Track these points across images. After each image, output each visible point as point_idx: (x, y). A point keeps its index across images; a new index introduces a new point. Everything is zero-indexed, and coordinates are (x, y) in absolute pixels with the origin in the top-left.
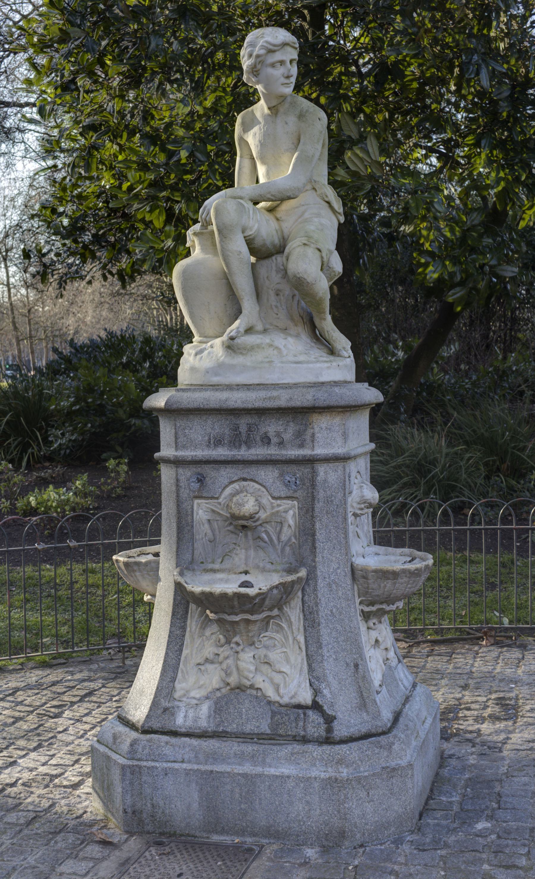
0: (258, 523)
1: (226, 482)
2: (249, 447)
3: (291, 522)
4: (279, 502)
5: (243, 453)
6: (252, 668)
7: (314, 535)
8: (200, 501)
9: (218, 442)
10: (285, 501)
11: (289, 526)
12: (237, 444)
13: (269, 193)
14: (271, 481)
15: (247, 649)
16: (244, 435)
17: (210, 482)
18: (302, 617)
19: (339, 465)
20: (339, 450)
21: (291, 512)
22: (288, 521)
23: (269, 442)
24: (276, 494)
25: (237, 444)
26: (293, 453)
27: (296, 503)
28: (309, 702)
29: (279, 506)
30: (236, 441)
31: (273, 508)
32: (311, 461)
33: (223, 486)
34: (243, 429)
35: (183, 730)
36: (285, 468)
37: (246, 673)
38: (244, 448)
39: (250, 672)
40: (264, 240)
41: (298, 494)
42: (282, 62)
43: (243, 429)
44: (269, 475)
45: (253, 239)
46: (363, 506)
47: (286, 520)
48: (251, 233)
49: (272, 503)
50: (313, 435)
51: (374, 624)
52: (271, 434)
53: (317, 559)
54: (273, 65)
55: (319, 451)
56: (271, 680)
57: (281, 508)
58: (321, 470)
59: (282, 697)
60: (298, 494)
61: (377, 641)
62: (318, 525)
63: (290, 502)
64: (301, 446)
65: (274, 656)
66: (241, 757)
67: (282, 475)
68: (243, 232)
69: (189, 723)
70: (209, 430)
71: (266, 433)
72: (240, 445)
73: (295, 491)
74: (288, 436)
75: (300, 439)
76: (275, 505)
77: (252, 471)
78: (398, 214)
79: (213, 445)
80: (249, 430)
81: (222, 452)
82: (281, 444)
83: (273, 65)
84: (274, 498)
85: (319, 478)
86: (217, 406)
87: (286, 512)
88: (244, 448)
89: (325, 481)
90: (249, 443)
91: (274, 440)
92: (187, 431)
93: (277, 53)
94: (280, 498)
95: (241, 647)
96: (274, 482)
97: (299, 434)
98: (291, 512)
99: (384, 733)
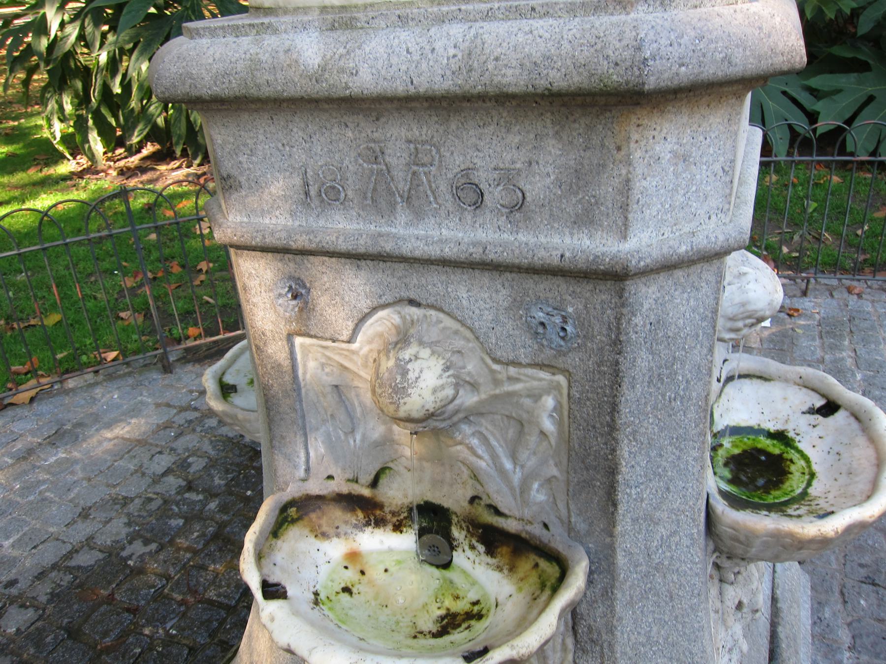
2: (419, 215)
3: (548, 425)
4: (512, 371)
5: (410, 234)
7: (612, 471)
8: (308, 341)
10: (530, 371)
11: (543, 433)
12: (383, 204)
14: (488, 316)
16: (399, 174)
22: (538, 424)
23: (479, 201)
25: (383, 204)
26: (556, 240)
27: (561, 379)
29: (510, 379)
30: (379, 196)
32: (614, 277)
34: (397, 156)
36: (530, 284)
38: (402, 216)
41: (573, 360)
43: (397, 156)
44: (480, 299)
49: (492, 372)
52: (482, 177)
55: (642, 242)
57: (518, 387)
60: (573, 360)
62: (625, 450)
64: (586, 219)
66: (498, 441)
67: (517, 304)
70: (299, 156)
71: (467, 172)
72: (393, 206)
73: (560, 353)
74: (537, 186)
75: (594, 198)
76: (502, 376)
77: (434, 284)
78: (421, 343)
79: (316, 202)
80: (415, 160)
81: (343, 227)
82: (518, 208)
84: (496, 360)
85: (638, 320)
86: (577, 80)
87: (536, 397)
88: (402, 216)
89: (659, 323)
90: (415, 201)
91: (495, 195)
92: (243, 159)
96: (496, 320)
97: (578, 180)
98: (549, 402)
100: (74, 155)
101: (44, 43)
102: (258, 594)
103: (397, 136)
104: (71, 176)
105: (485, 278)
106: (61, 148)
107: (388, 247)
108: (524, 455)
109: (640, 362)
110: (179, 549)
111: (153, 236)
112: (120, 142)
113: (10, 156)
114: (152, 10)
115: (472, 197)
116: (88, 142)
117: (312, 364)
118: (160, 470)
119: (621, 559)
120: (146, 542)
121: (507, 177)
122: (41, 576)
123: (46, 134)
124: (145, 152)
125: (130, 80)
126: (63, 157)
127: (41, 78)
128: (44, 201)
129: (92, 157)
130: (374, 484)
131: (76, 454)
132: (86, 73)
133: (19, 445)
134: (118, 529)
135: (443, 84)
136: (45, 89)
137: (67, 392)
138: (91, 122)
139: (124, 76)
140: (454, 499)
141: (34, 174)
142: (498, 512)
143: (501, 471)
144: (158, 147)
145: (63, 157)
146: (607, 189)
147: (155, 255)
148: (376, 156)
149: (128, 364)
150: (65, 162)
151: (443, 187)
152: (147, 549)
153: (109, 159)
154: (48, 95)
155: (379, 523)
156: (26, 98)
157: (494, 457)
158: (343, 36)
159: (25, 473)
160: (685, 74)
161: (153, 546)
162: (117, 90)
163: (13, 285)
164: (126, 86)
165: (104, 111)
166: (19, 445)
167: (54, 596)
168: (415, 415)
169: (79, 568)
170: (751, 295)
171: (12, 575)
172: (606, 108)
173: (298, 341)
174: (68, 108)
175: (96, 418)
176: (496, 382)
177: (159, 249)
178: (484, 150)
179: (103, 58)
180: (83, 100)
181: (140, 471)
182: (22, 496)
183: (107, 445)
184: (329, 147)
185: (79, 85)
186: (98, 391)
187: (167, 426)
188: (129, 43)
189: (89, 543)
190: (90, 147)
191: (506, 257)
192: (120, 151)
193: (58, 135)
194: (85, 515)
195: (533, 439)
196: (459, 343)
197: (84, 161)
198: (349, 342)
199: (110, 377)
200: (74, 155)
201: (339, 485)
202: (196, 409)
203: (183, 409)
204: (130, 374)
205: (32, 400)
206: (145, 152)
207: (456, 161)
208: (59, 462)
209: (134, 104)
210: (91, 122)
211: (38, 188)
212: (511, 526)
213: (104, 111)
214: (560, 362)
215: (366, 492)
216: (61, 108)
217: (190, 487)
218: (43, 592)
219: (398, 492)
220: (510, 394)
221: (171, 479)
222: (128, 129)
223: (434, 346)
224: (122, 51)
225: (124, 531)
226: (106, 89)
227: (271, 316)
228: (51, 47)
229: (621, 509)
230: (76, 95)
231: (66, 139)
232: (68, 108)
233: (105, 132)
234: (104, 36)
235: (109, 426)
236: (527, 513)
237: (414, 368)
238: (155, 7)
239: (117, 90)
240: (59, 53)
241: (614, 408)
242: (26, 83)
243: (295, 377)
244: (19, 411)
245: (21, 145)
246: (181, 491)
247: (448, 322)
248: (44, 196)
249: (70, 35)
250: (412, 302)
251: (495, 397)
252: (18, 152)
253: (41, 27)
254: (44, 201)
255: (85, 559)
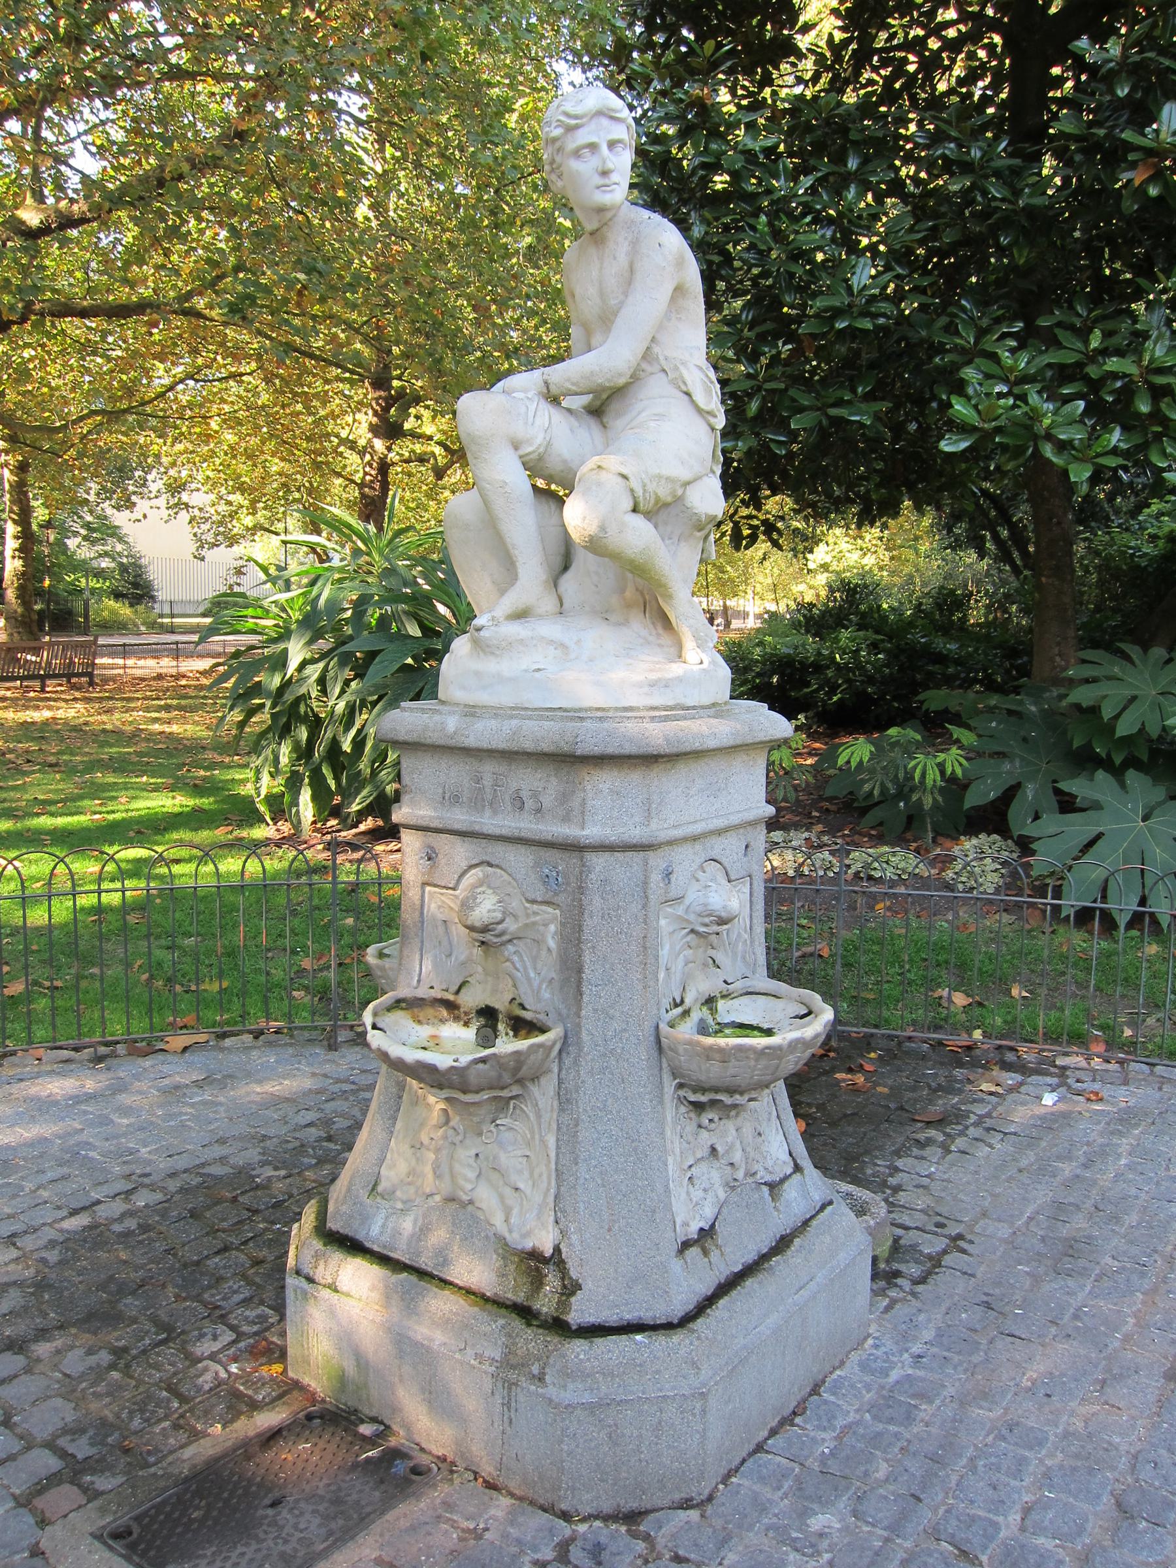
0: (505, 938)
1: (464, 865)
2: (495, 813)
3: (552, 943)
5: (490, 823)
6: (471, 1175)
7: (580, 971)
9: (455, 799)
10: (543, 908)
11: (549, 950)
13: (568, 380)
14: (523, 871)
15: (467, 1141)
16: (488, 790)
17: (443, 862)
18: (556, 1103)
19: (637, 857)
20: (635, 833)
21: (552, 928)
24: (531, 896)
28: (548, 1252)
30: (478, 802)
31: (528, 916)
33: (460, 871)
34: (487, 781)
35: (376, 1248)
37: (462, 1182)
38: (488, 812)
39: (467, 1180)
40: (565, 462)
42: (593, 147)
44: (519, 860)
45: (541, 458)
46: (707, 920)
47: (544, 941)
48: (530, 449)
50: (583, 802)
51: (711, 1121)
52: (525, 794)
53: (583, 1013)
54: (577, 153)
55: (592, 832)
56: (502, 1198)
58: (599, 862)
59: (510, 1231)
60: (561, 899)
61: (713, 1150)
62: (587, 958)
63: (550, 910)
64: (566, 819)
65: (510, 1159)
67: (537, 864)
68: (516, 448)
69: (385, 1238)
73: (556, 894)
74: (547, 800)
77: (499, 852)
78: (489, 887)
81: (460, 818)
83: (577, 153)
84: (528, 901)
88: (488, 812)
90: (494, 805)
91: (529, 804)
93: (581, 131)
94: (533, 902)
95: (460, 1138)
97: (564, 798)
98: (552, 928)
99: (669, 1327)
100: (275, 820)
101: (276, 681)
102: (369, 1028)
103: (489, 769)
104: (267, 842)
105: (522, 849)
106: (262, 808)
107: (477, 828)
108: (539, 965)
109: (595, 902)
110: (305, 1180)
111: (350, 921)
112: (336, 812)
113: (197, 811)
114: (410, 661)
115: (518, 804)
116: (297, 805)
117: (433, 906)
118: (303, 1122)
119: (585, 1036)
120: (276, 1169)
121: (535, 795)
122: (173, 1175)
123: (248, 790)
124: (362, 827)
125: (365, 737)
126: (262, 820)
127: (263, 719)
128: (231, 865)
129: (297, 826)
130: (457, 992)
131: (221, 1099)
132: (316, 724)
133: (166, 1082)
134: (253, 1154)
135: (502, 746)
136: (263, 735)
137: (222, 1049)
138: (307, 780)
139: (359, 731)
140: (500, 1003)
141: (220, 834)
142: (524, 1008)
143: (529, 979)
144: (380, 823)
145: (262, 820)
146: (575, 803)
147: (347, 939)
148: (478, 780)
149: (292, 1036)
150: (263, 826)
151: (507, 798)
152: (277, 1173)
153: (316, 830)
154: (264, 743)
155: (457, 1019)
156: (231, 747)
157: (525, 968)
158: (468, 719)
159: (170, 1103)
160: (597, 750)
161: (283, 1173)
162: (347, 747)
163: (180, 948)
164: (359, 744)
165: (326, 771)
166: (166, 1082)
167: (181, 1190)
168: (478, 924)
169: (209, 1175)
170: (711, 900)
171: (148, 1170)
172: (573, 763)
173: (428, 889)
174: (284, 760)
175: (248, 1075)
176: (528, 916)
177: (353, 935)
178: (527, 780)
179: (341, 706)
180: (304, 753)
181: (284, 1120)
182: (164, 1121)
183: (254, 1097)
184: (455, 773)
185: (303, 734)
186: (255, 1053)
187: (318, 1092)
188: (372, 694)
189: (223, 1160)
190: (298, 812)
191: (529, 835)
192: (333, 822)
193: (264, 792)
194: (222, 1141)
195: (544, 953)
196: (509, 890)
197: (286, 828)
198: (454, 889)
199: (270, 1044)
200: (275, 820)
201: (437, 993)
202: (353, 1083)
203: (338, 1081)
204: (291, 1045)
205: (185, 1049)
206: (362, 827)
207: (514, 785)
208: (204, 1103)
209: (364, 766)
210: (307, 780)
211: (226, 851)
212: (528, 1015)
213: (326, 771)
214: (555, 900)
215: (451, 997)
216: (276, 760)
217: (329, 1139)
218: (173, 1185)
219: (471, 999)
220: (534, 923)
221: (313, 1130)
222: (348, 794)
223: (495, 890)
224: (363, 703)
225: (257, 1158)
226: (335, 744)
227: (415, 871)
228: (286, 685)
229: (586, 998)
230: (296, 747)
231: (273, 801)
232: (284, 760)
233: (321, 795)
234: (347, 683)
235: (260, 1082)
236: (539, 1007)
237: (480, 898)
238: (413, 658)
239: (347, 747)
240: (289, 697)
241: (581, 930)
242: (242, 725)
243: (422, 913)
244: (169, 1057)
245: (212, 799)
246: (320, 1140)
247: (506, 876)
248: (230, 860)
249: (308, 677)
250: (490, 865)
251: (526, 925)
252: (206, 807)
253: (280, 661)
254: (231, 865)
255: (217, 1170)
